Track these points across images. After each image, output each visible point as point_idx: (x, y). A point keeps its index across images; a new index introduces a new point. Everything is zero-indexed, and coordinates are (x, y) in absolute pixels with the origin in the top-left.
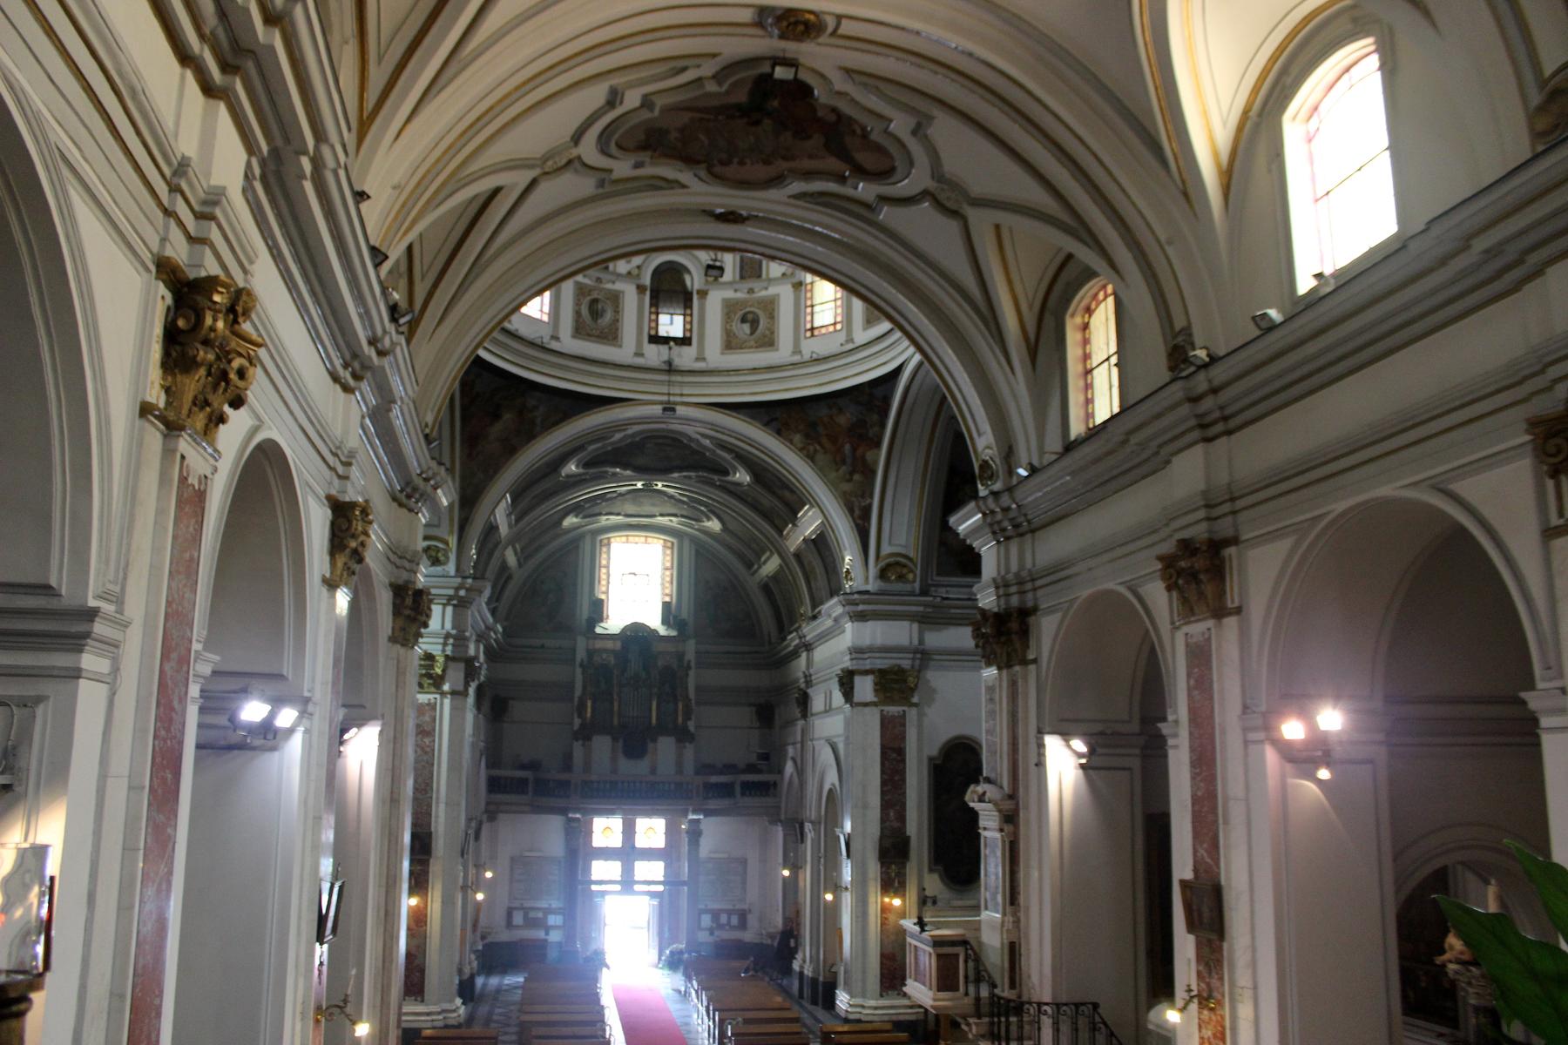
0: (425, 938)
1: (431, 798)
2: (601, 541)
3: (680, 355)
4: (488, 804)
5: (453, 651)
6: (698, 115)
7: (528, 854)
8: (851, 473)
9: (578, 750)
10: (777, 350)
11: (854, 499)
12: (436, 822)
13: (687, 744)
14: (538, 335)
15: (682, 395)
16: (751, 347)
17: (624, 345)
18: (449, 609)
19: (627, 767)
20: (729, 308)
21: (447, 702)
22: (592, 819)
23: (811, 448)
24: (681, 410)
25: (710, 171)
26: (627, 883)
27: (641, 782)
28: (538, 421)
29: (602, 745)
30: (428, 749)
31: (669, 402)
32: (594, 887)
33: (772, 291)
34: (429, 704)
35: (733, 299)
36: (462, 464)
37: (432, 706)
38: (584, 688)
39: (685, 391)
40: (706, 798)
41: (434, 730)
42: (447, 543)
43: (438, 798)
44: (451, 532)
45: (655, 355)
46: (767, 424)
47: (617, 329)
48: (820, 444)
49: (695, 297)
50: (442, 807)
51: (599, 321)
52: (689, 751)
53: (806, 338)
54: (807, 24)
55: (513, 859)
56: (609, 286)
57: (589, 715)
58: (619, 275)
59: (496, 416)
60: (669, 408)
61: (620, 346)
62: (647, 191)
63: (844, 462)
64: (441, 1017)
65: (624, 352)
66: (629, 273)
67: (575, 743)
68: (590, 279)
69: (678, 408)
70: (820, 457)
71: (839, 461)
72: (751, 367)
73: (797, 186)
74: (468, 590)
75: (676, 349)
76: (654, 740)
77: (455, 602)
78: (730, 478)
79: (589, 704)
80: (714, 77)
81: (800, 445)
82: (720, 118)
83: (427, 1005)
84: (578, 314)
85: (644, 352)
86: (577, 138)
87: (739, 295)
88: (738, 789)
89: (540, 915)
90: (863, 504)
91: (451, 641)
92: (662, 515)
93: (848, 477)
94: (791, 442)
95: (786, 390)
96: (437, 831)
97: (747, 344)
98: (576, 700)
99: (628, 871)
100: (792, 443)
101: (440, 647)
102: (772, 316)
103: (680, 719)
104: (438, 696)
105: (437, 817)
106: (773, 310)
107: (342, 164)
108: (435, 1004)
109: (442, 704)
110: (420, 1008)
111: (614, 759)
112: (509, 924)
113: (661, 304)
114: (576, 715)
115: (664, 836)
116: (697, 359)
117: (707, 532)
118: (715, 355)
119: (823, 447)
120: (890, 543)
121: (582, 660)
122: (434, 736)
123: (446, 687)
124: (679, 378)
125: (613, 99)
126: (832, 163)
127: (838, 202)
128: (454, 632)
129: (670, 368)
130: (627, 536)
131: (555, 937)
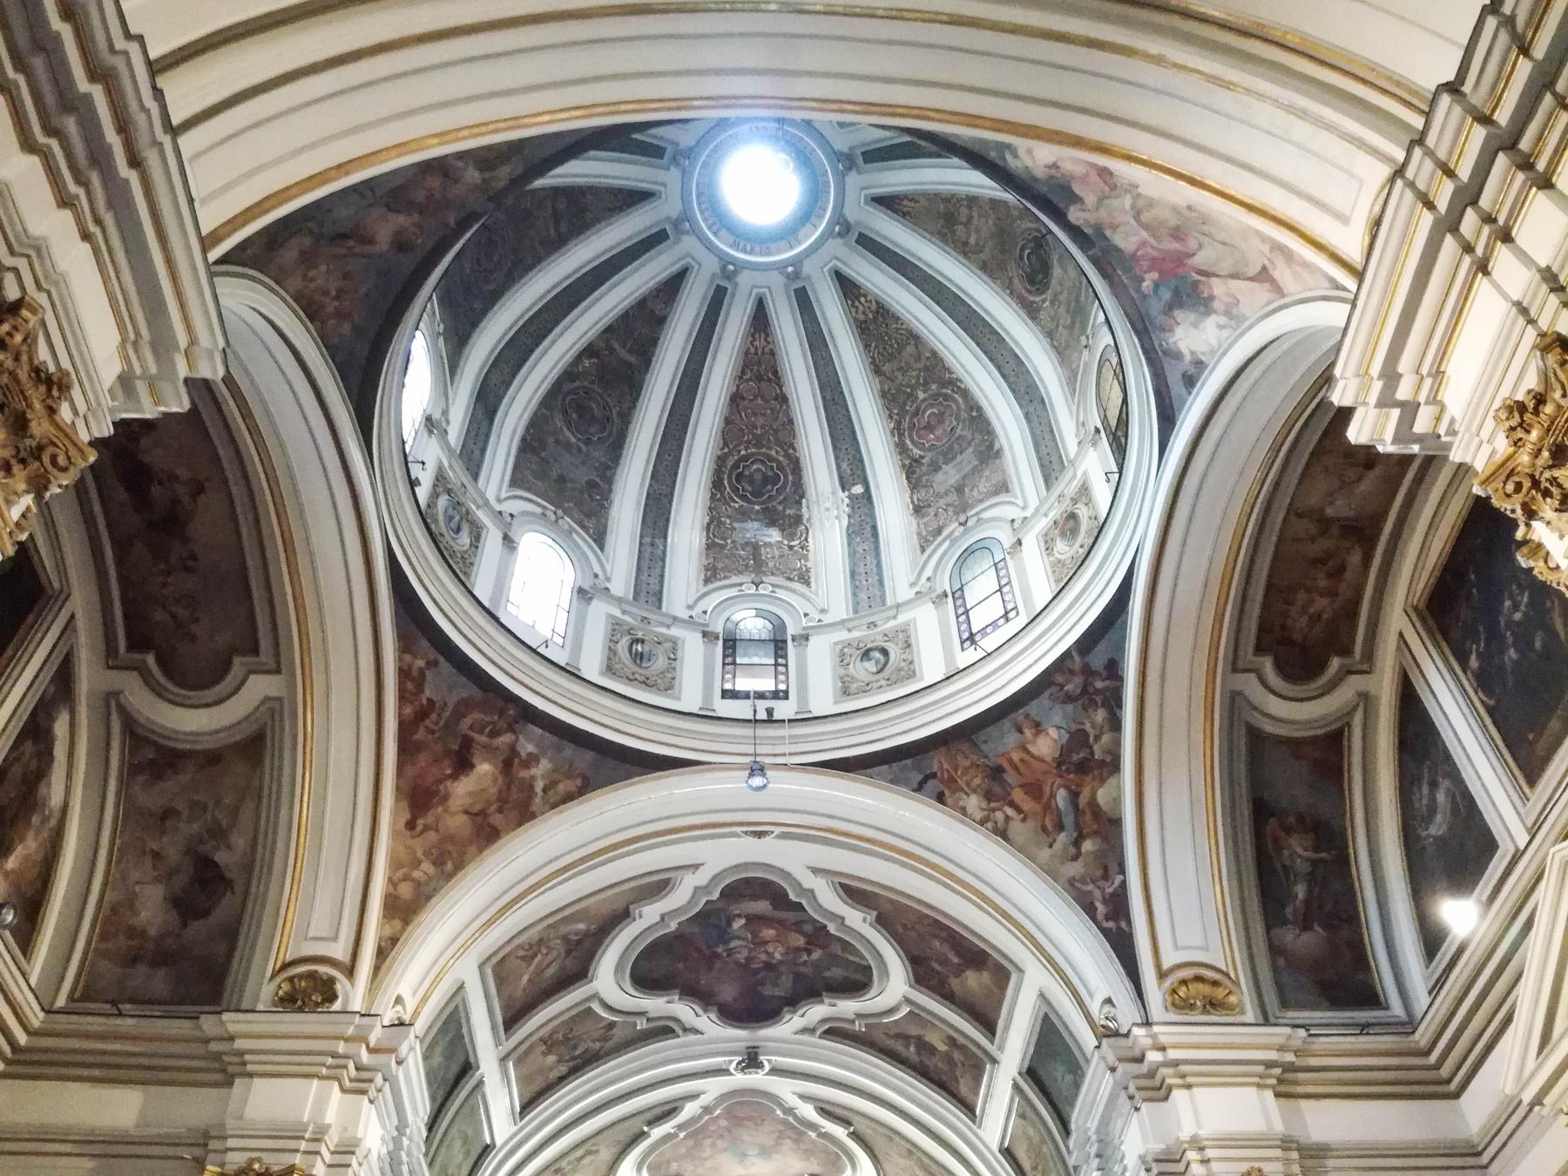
8: (1077, 843)
11: (1090, 887)
23: (999, 815)
28: (539, 786)
33: (903, 618)
48: (1012, 804)
59: (463, 764)
63: (1060, 827)
70: (1017, 828)
71: (1051, 825)
87: (855, 634)
90: (1110, 890)
93: (1073, 850)
107: (221, 347)
119: (1019, 810)
120: (1176, 947)
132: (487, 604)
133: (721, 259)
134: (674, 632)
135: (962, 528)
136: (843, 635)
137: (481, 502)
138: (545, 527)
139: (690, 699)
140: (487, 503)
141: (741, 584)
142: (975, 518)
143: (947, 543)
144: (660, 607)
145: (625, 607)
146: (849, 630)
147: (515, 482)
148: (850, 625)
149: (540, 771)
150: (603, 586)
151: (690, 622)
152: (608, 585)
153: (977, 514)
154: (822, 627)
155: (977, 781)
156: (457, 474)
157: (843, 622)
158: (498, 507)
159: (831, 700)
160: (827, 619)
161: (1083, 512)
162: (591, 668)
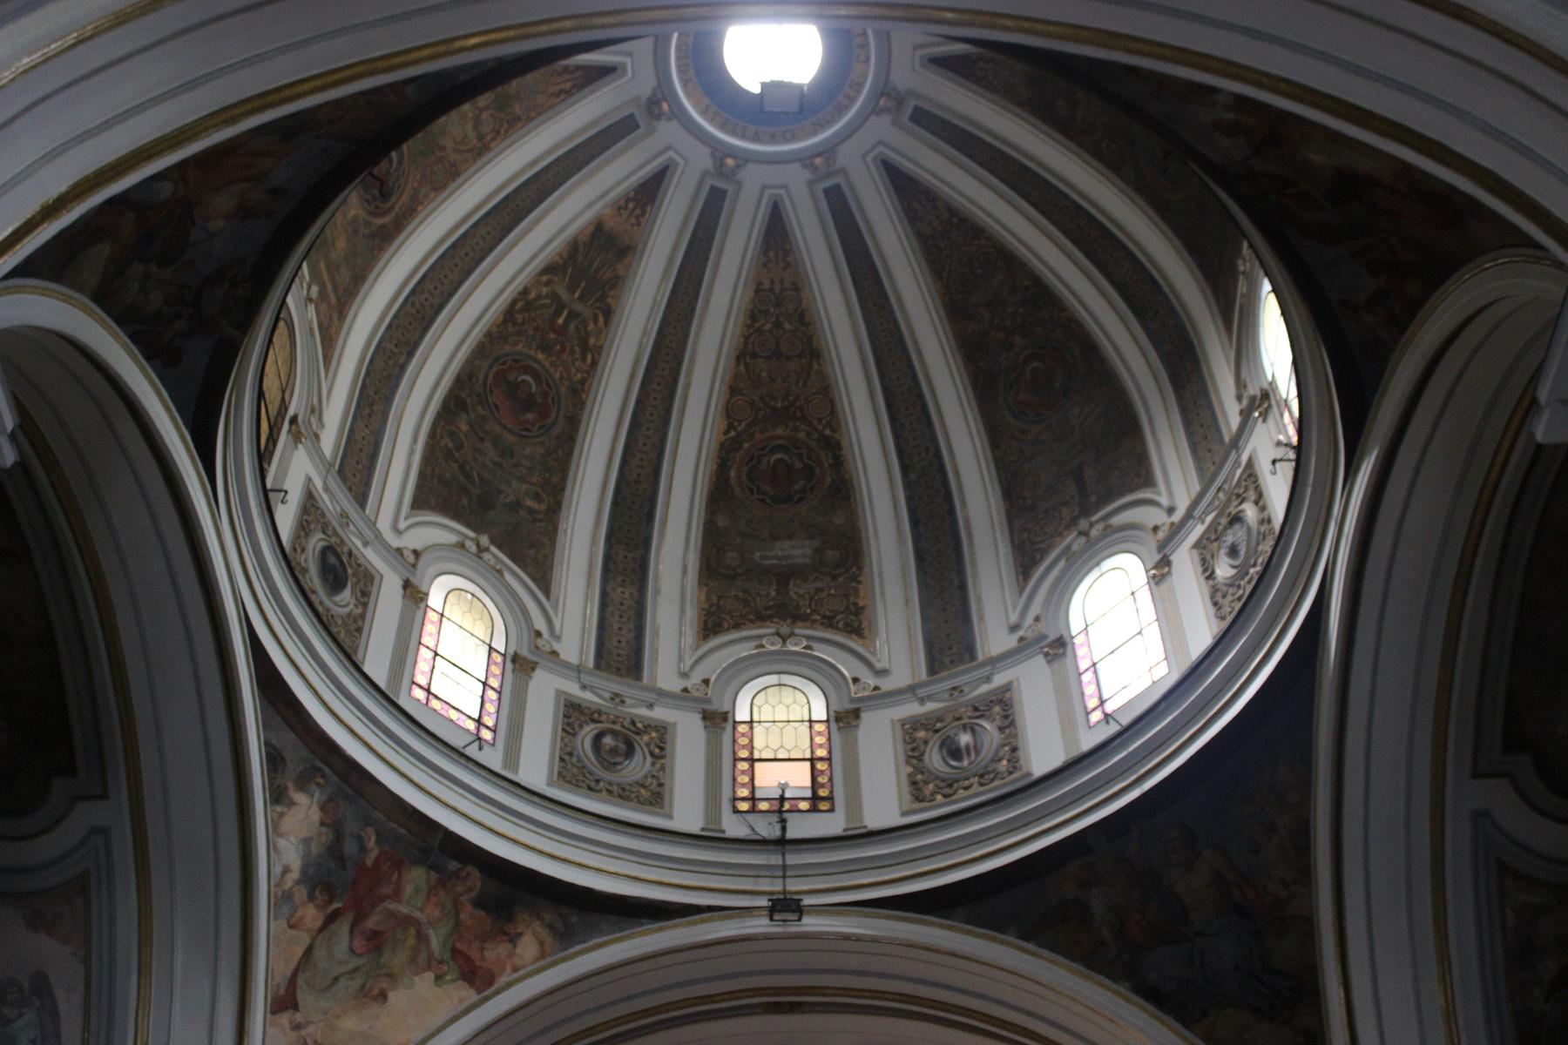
20: (914, 736)
66: (685, 690)
87: (930, 706)
132: (382, 684)
133: (800, 160)
135: (1082, 540)
136: (912, 709)
137: (369, 535)
138: (477, 572)
139: (687, 813)
140: (378, 535)
141: (760, 637)
142: (1100, 526)
143: (1062, 564)
144: (638, 677)
145: (586, 679)
147: (419, 503)
148: (921, 692)
150: (547, 648)
151: (684, 697)
152: (556, 646)
153: (1104, 518)
154: (879, 698)
156: (334, 501)
157: (911, 689)
158: (395, 542)
159: (897, 812)
160: (887, 684)
161: (1250, 512)
162: (535, 769)
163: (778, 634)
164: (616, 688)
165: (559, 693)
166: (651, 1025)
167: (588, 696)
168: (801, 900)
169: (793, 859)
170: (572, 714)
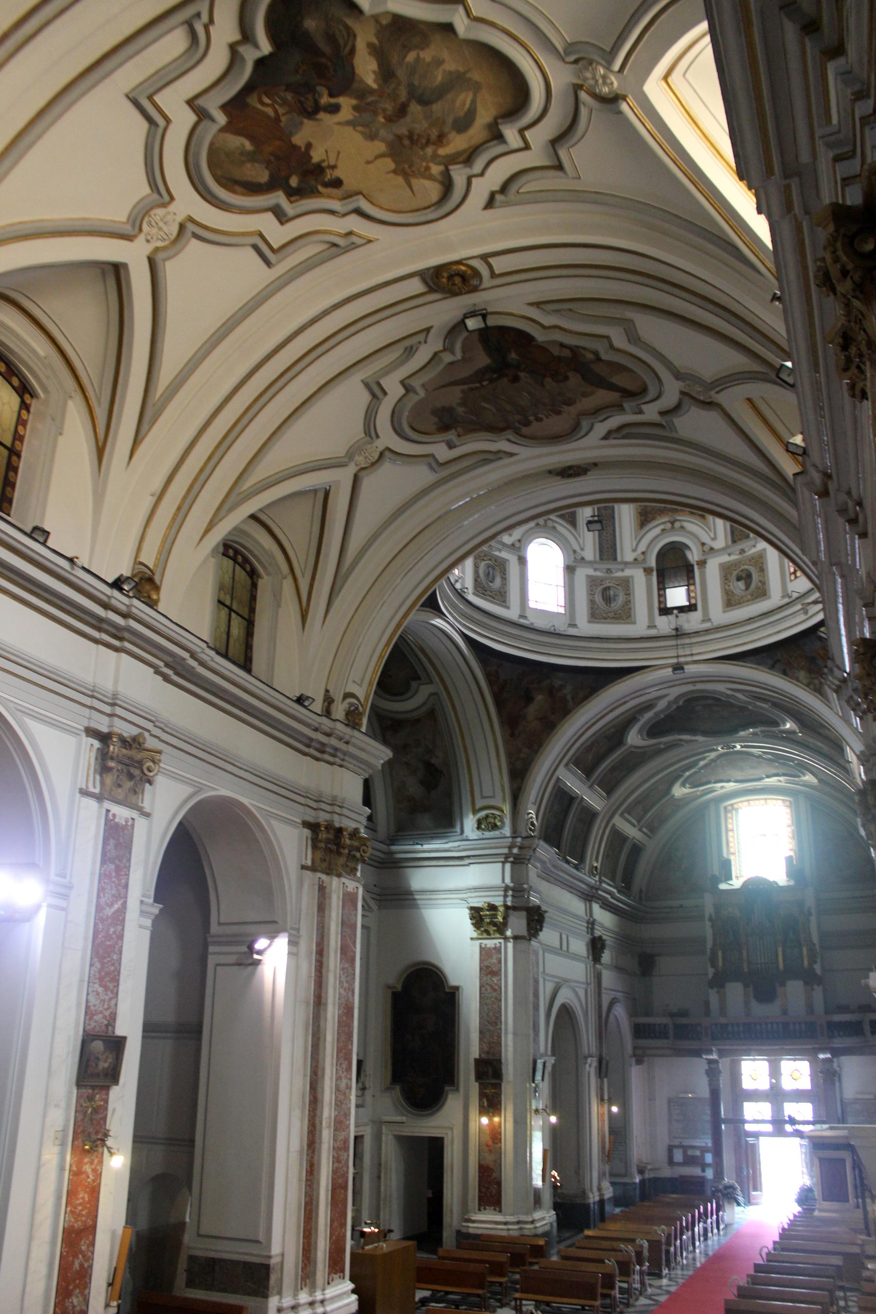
0: (501, 1153)
1: (501, 1029)
2: (725, 808)
3: (688, 621)
4: (635, 1048)
5: (512, 902)
6: (465, 387)
7: (681, 1095)
9: (713, 997)
10: (770, 598)
12: (506, 1050)
13: (816, 987)
14: (551, 624)
15: (692, 655)
16: (748, 601)
17: (638, 622)
18: (508, 866)
19: (760, 1010)
20: (726, 571)
21: (510, 945)
22: (739, 1061)
24: (690, 669)
25: (518, 433)
26: (779, 1124)
27: (766, 1024)
28: (569, 697)
29: (735, 991)
30: (496, 987)
31: (678, 663)
32: (748, 1127)
34: (495, 948)
35: (729, 562)
36: (506, 742)
37: (498, 950)
38: (715, 940)
39: (681, 652)
40: (831, 1037)
41: (500, 970)
42: (502, 811)
43: (506, 1030)
44: (504, 800)
45: (665, 624)
46: (772, 667)
47: (630, 609)
49: (696, 567)
50: (510, 1037)
51: (612, 605)
52: (818, 993)
53: (791, 581)
54: (463, 277)
55: (670, 1101)
56: (620, 574)
57: (720, 964)
58: (504, 545)
60: (678, 667)
61: (634, 623)
62: (481, 466)
64: (516, 1227)
65: (639, 627)
66: (635, 560)
67: (710, 991)
68: (602, 572)
69: (686, 667)
72: (747, 618)
73: (601, 429)
74: (520, 848)
75: (683, 616)
76: (783, 984)
77: (511, 859)
78: (782, 728)
79: (720, 954)
80: (445, 350)
81: (805, 681)
82: (485, 383)
83: (505, 1215)
84: (592, 602)
85: (657, 624)
86: (370, 430)
88: (867, 1028)
89: (698, 1153)
91: (510, 893)
92: (768, 777)
94: (798, 680)
95: (779, 632)
96: (506, 1059)
97: (745, 598)
98: (708, 950)
99: (778, 1109)
100: (798, 681)
101: (501, 899)
102: (762, 570)
103: (806, 963)
104: (502, 941)
105: (506, 1046)
106: (762, 563)
108: (511, 1215)
109: (506, 948)
110: (499, 1218)
111: (747, 1003)
112: (671, 1162)
113: (666, 581)
114: (709, 965)
115: (809, 1078)
116: (703, 621)
117: (806, 785)
118: (718, 614)
121: (711, 915)
122: (501, 975)
123: (509, 933)
124: (687, 641)
125: (376, 391)
126: (602, 396)
127: (635, 430)
128: (511, 885)
129: (678, 634)
130: (748, 801)
131: (709, 1174)
134: (628, 572)
136: (725, 558)
144: (615, 559)
145: (596, 566)
146: (729, 555)
149: (568, 691)
155: (803, 664)
163: (669, 522)
164: (609, 566)
165: (588, 576)
166: (350, 1026)
167: (598, 574)
168: (867, 399)
169: (90, 693)
170: (592, 582)
